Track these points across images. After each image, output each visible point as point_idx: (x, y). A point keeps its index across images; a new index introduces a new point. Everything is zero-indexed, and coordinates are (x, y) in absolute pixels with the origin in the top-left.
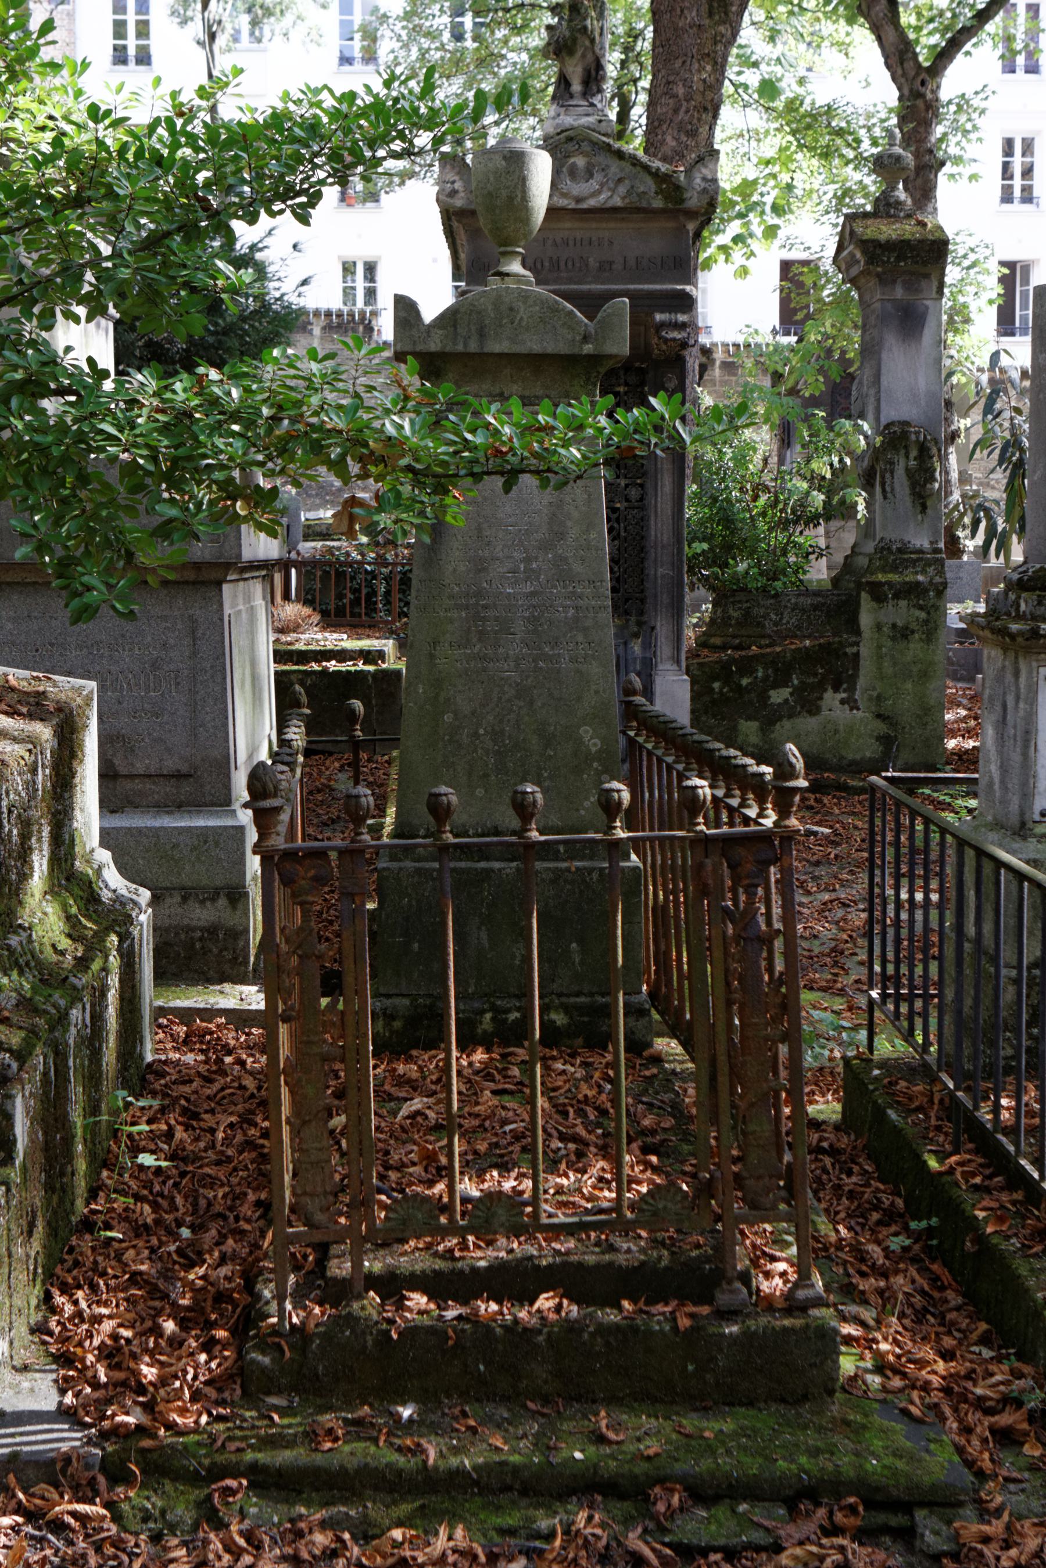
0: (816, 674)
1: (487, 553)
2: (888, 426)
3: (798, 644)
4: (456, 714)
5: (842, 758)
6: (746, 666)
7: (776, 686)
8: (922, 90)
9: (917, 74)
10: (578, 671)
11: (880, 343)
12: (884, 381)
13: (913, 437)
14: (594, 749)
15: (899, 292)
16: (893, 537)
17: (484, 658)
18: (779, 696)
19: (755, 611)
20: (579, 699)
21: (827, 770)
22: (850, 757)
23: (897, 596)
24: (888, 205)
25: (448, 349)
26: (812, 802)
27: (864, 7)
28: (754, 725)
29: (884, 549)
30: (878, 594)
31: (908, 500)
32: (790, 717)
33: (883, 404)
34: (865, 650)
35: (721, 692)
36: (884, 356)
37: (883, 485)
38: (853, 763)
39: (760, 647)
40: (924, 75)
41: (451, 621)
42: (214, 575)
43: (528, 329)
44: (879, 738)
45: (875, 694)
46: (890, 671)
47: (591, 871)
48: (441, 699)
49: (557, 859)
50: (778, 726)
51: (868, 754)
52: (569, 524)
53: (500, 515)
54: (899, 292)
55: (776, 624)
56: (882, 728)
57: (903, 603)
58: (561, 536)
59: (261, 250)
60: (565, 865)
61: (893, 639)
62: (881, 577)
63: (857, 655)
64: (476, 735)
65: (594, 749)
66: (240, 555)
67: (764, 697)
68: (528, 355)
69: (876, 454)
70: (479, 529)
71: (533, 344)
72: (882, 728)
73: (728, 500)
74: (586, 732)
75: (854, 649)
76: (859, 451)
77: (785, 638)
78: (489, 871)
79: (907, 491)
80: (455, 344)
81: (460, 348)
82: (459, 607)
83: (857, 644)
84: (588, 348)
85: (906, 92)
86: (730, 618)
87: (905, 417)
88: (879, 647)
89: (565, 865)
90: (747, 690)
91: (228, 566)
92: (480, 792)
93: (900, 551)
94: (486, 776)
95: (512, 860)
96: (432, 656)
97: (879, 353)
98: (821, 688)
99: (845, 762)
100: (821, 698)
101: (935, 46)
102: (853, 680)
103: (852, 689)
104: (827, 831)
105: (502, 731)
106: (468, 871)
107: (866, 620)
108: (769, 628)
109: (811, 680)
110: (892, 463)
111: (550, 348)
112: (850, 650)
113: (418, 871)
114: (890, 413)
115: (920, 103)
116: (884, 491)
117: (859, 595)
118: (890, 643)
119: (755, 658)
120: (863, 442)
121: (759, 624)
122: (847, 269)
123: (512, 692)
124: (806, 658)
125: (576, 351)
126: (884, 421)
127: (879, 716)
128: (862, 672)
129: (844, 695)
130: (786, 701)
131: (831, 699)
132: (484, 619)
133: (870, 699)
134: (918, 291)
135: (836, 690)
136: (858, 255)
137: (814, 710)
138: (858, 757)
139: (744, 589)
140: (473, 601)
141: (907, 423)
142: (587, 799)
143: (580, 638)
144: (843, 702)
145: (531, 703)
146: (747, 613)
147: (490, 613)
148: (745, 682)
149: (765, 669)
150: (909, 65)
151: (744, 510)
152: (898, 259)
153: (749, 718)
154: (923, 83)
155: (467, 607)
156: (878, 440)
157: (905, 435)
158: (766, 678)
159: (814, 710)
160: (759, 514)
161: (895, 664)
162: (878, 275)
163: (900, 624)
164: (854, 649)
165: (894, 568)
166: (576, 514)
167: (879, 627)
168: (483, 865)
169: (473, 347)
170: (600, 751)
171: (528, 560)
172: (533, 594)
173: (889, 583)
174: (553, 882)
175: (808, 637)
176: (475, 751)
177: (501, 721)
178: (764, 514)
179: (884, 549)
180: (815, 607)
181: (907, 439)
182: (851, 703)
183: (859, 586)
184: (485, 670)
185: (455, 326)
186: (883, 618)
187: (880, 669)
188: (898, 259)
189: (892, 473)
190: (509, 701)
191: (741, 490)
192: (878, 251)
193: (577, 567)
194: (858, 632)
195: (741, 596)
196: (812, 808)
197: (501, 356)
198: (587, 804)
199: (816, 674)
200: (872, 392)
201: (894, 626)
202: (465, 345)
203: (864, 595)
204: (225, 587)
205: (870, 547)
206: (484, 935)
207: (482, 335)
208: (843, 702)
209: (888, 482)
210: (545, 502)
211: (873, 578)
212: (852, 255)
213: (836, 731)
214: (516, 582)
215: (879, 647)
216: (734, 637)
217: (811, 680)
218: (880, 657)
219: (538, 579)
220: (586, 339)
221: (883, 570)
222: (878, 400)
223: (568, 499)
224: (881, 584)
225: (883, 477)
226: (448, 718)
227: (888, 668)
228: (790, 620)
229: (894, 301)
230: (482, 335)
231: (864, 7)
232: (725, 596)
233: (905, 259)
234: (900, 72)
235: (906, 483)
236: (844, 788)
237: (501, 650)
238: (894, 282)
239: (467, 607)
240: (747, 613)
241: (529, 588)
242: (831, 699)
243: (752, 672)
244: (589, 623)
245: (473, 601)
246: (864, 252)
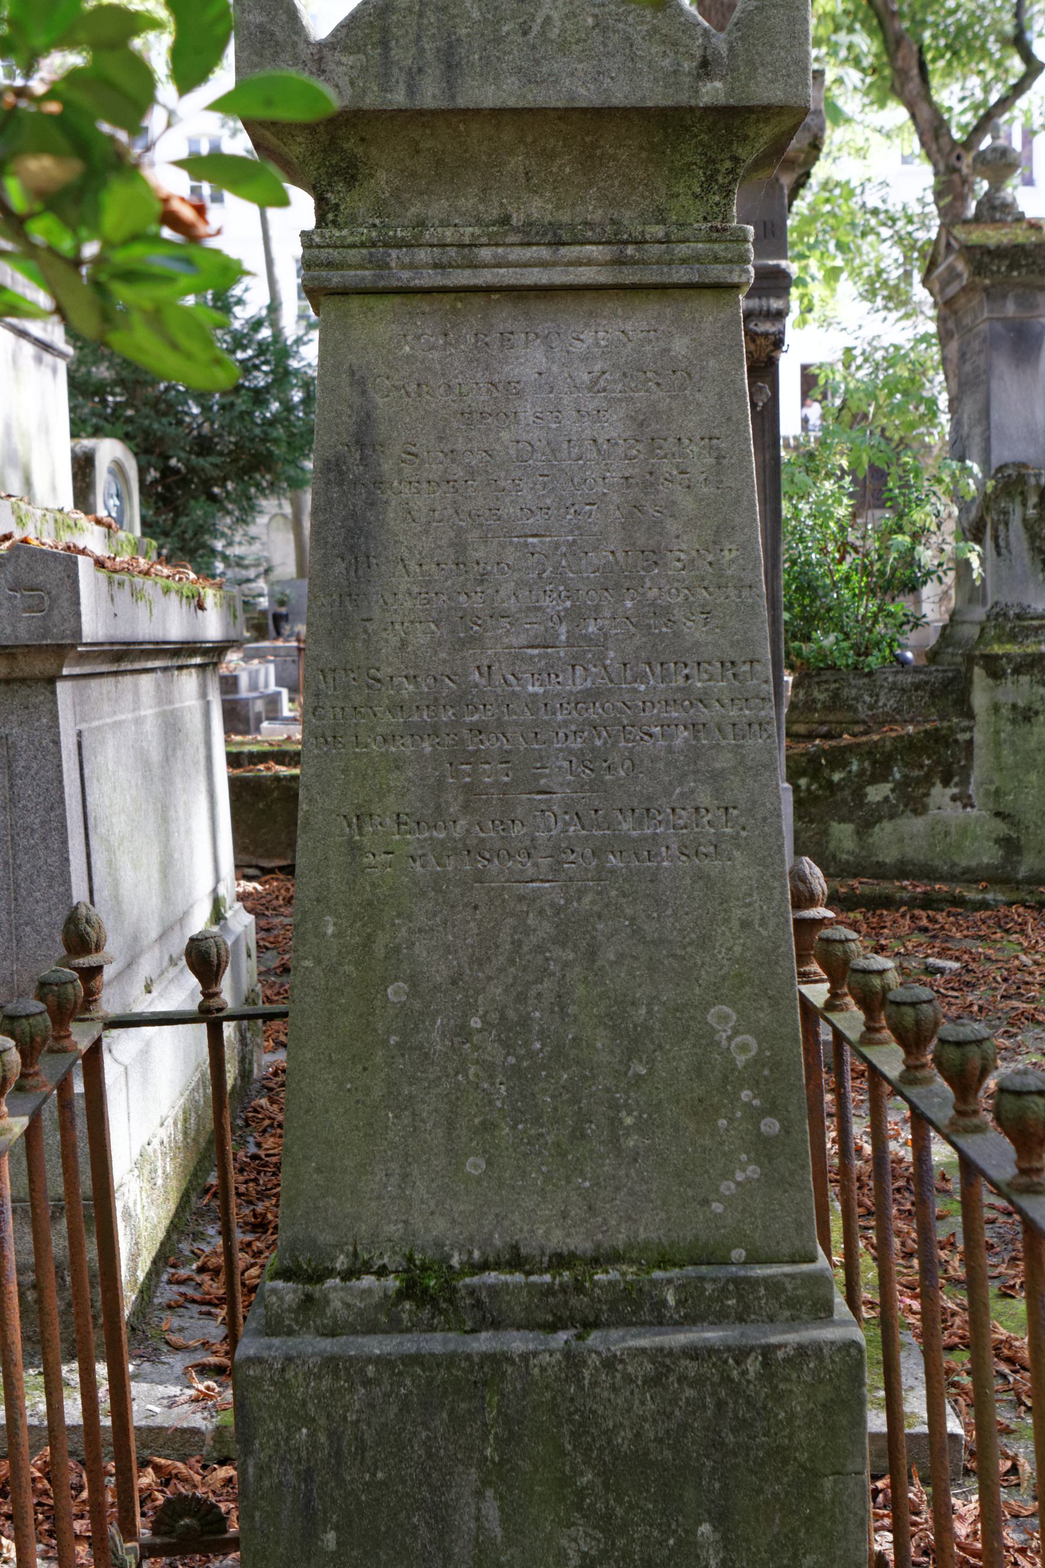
0: (921, 766)
1: (477, 602)
2: (1000, 469)
3: (900, 731)
4: (413, 981)
5: (954, 865)
6: (838, 758)
7: (874, 780)
8: (958, 164)
9: (952, 150)
10: (700, 876)
11: (988, 371)
12: (995, 416)
13: (1032, 481)
14: (741, 1060)
15: (1010, 309)
16: (1011, 599)
17: (474, 850)
18: (876, 793)
19: (845, 692)
20: (705, 942)
21: (938, 880)
22: (964, 863)
23: (1017, 671)
24: (993, 208)
25: (370, 102)
26: (924, 922)
27: (897, 86)
28: (849, 828)
29: (998, 615)
30: (994, 668)
31: (1027, 556)
32: (891, 817)
33: (994, 443)
34: (980, 737)
35: (808, 789)
36: (994, 385)
37: (996, 538)
38: (967, 871)
39: (854, 735)
40: (959, 150)
41: (398, 764)
42: (39, 666)
43: (563, 47)
44: (997, 841)
45: (993, 788)
46: (1010, 760)
47: (741, 1354)
48: (379, 949)
49: (660, 1320)
50: (877, 829)
51: (985, 860)
52: (673, 527)
53: (509, 510)
54: (1010, 309)
55: (871, 707)
56: (1002, 828)
57: (1025, 679)
58: (654, 557)
59: (305, 344)
60: (680, 1338)
61: (1014, 722)
62: (997, 649)
63: (970, 742)
64: (463, 1032)
65: (741, 1060)
66: (78, 632)
67: (859, 795)
68: (565, 114)
69: (987, 502)
70: (460, 546)
71: (576, 85)
72: (1002, 828)
73: (808, 563)
74: (722, 1018)
75: (967, 736)
76: (968, 498)
77: (883, 724)
78: (496, 1360)
79: (1026, 545)
80: (385, 89)
81: (399, 98)
82: (416, 732)
83: (970, 729)
84: (713, 91)
85: (942, 167)
86: (814, 701)
87: (1021, 457)
88: (997, 732)
89: (680, 1338)
90: (839, 787)
91: (61, 651)
92: (475, 1165)
93: (1019, 617)
94: (488, 1127)
95: (553, 1327)
96: (354, 849)
97: (988, 383)
98: (927, 780)
99: (957, 870)
100: (927, 795)
101: (968, 124)
102: (966, 773)
103: (965, 782)
104: (956, 965)
105: (525, 1021)
106: (451, 1360)
107: (980, 699)
108: (863, 712)
109: (916, 773)
110: (1006, 513)
111: (620, 93)
112: (962, 737)
113: (331, 1363)
114: (1001, 454)
115: (956, 177)
116: (997, 546)
117: (970, 670)
118: (1009, 728)
119: (849, 748)
120: (973, 487)
121: (850, 708)
122: (942, 290)
123: (546, 929)
124: (909, 747)
125: (683, 99)
126: (995, 463)
127: (998, 814)
128: (977, 763)
129: (956, 790)
130: (886, 799)
131: (940, 794)
132: (475, 758)
133: (987, 793)
134: (1033, 307)
135: (946, 783)
136: (961, 266)
137: (919, 808)
138: (973, 863)
139: (833, 667)
140: (447, 716)
141: (1024, 465)
142: (727, 1174)
143: (704, 797)
144: (954, 798)
145: (592, 954)
146: (836, 695)
147: (491, 744)
148: (836, 777)
149: (861, 761)
150: (944, 141)
151: (824, 575)
152: (1011, 268)
153: (842, 820)
154: (959, 158)
155: (435, 731)
156: (990, 484)
157: (1021, 479)
158: (862, 772)
159: (919, 808)
160: (841, 579)
161: (1016, 752)
162: (986, 289)
163: (1021, 704)
164: (967, 736)
165: (1013, 637)
166: (687, 503)
167: (996, 708)
168: (484, 1342)
169: (431, 95)
170: (756, 1062)
171: (576, 615)
172: (592, 696)
173: (1008, 656)
174: (654, 1381)
175: (911, 721)
176: (461, 1069)
177: (521, 998)
178: (847, 579)
179: (998, 615)
180: (917, 687)
181: (1025, 483)
182: (964, 800)
183: (970, 660)
184: (480, 877)
185: (384, 44)
186: (1002, 699)
187: (998, 757)
188: (1011, 268)
189: (1007, 524)
190: (539, 949)
191: (823, 551)
192: (986, 259)
193: (694, 630)
194: (970, 715)
195: (827, 675)
196: (925, 930)
197: (498, 114)
198: (727, 1187)
199: (921, 766)
200: (978, 430)
201: (1014, 707)
202: (411, 91)
203: (978, 672)
204: (63, 689)
205: (979, 613)
206: (491, 1509)
207: (451, 65)
208: (954, 798)
209: (1002, 536)
210: (614, 477)
211: (987, 651)
212: (951, 269)
213: (947, 834)
214: (550, 670)
215: (997, 732)
216: (822, 723)
217: (916, 773)
218: (998, 744)
219: (601, 658)
220: (706, 67)
221: (999, 639)
222: (987, 440)
223: (667, 467)
224: (997, 657)
225: (995, 530)
226: (396, 992)
227: (1008, 757)
228: (887, 702)
229: (1004, 320)
230: (451, 65)
231: (897, 86)
232: (808, 675)
233: (1019, 267)
234: (934, 148)
235: (1024, 536)
236: (958, 902)
237: (517, 830)
238: (1004, 296)
239: (435, 731)
240: (836, 695)
241: (580, 682)
242: (940, 794)
243: (844, 765)
244: (724, 761)
245: (447, 716)
246: (969, 261)
